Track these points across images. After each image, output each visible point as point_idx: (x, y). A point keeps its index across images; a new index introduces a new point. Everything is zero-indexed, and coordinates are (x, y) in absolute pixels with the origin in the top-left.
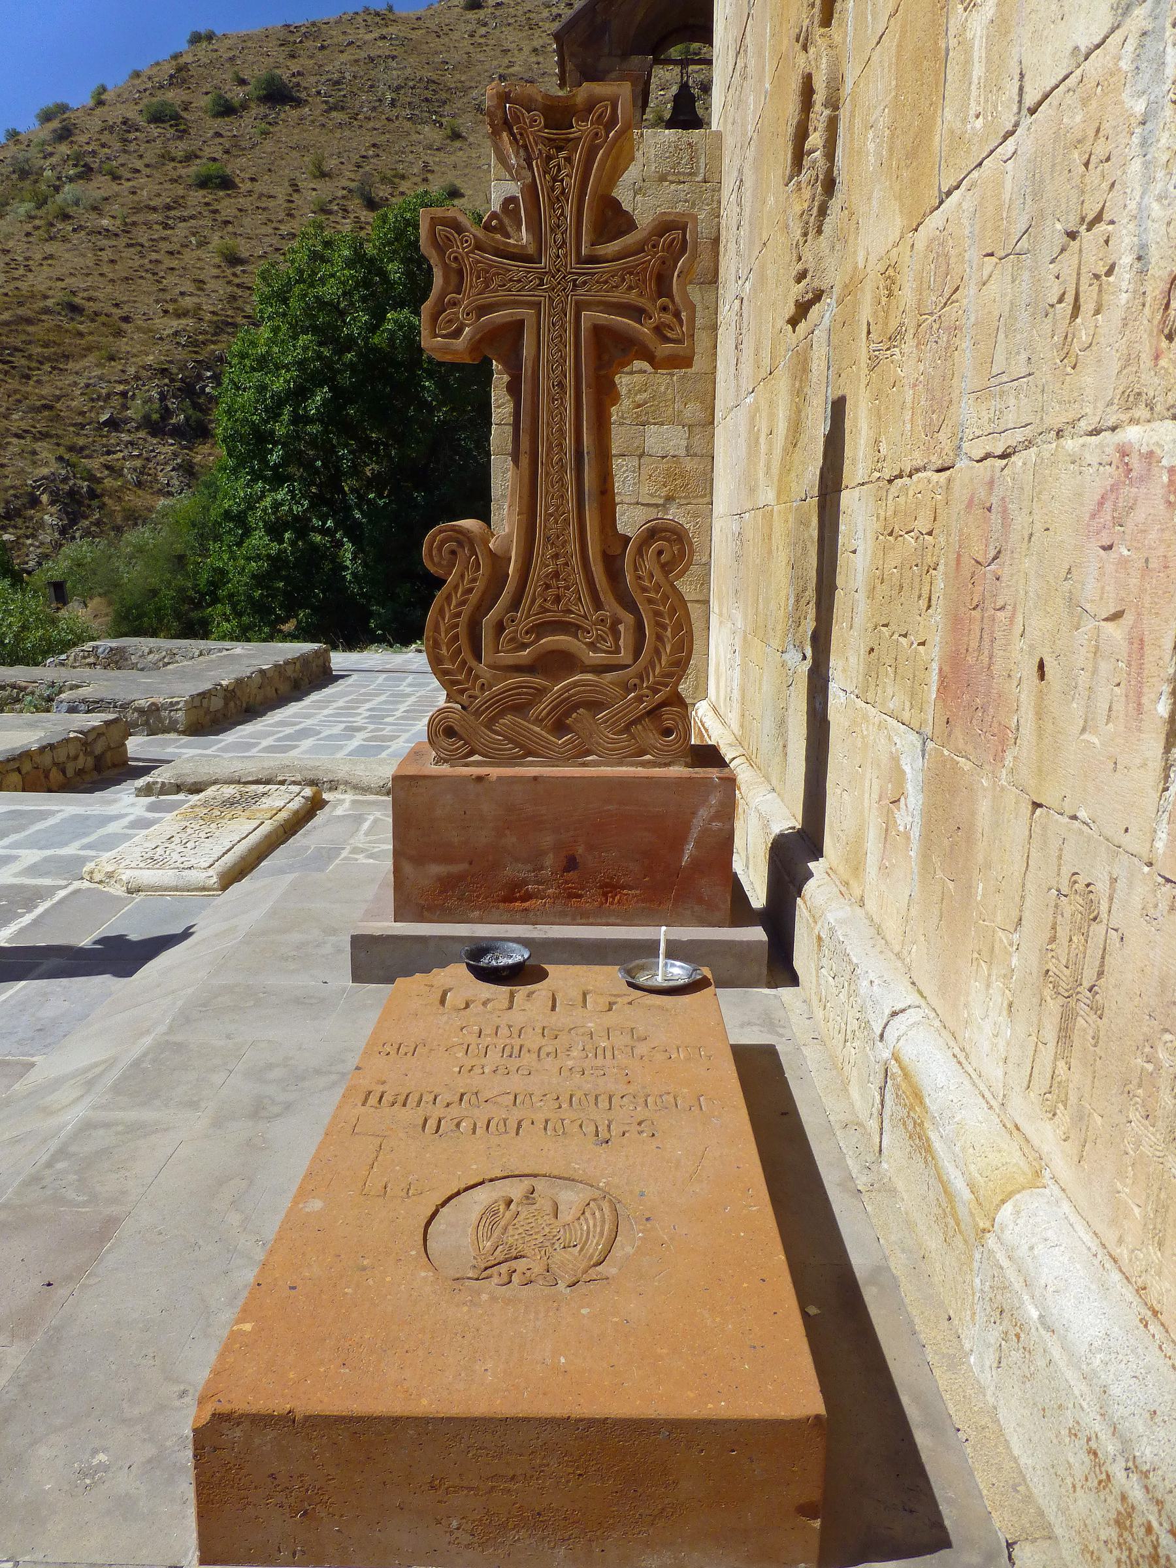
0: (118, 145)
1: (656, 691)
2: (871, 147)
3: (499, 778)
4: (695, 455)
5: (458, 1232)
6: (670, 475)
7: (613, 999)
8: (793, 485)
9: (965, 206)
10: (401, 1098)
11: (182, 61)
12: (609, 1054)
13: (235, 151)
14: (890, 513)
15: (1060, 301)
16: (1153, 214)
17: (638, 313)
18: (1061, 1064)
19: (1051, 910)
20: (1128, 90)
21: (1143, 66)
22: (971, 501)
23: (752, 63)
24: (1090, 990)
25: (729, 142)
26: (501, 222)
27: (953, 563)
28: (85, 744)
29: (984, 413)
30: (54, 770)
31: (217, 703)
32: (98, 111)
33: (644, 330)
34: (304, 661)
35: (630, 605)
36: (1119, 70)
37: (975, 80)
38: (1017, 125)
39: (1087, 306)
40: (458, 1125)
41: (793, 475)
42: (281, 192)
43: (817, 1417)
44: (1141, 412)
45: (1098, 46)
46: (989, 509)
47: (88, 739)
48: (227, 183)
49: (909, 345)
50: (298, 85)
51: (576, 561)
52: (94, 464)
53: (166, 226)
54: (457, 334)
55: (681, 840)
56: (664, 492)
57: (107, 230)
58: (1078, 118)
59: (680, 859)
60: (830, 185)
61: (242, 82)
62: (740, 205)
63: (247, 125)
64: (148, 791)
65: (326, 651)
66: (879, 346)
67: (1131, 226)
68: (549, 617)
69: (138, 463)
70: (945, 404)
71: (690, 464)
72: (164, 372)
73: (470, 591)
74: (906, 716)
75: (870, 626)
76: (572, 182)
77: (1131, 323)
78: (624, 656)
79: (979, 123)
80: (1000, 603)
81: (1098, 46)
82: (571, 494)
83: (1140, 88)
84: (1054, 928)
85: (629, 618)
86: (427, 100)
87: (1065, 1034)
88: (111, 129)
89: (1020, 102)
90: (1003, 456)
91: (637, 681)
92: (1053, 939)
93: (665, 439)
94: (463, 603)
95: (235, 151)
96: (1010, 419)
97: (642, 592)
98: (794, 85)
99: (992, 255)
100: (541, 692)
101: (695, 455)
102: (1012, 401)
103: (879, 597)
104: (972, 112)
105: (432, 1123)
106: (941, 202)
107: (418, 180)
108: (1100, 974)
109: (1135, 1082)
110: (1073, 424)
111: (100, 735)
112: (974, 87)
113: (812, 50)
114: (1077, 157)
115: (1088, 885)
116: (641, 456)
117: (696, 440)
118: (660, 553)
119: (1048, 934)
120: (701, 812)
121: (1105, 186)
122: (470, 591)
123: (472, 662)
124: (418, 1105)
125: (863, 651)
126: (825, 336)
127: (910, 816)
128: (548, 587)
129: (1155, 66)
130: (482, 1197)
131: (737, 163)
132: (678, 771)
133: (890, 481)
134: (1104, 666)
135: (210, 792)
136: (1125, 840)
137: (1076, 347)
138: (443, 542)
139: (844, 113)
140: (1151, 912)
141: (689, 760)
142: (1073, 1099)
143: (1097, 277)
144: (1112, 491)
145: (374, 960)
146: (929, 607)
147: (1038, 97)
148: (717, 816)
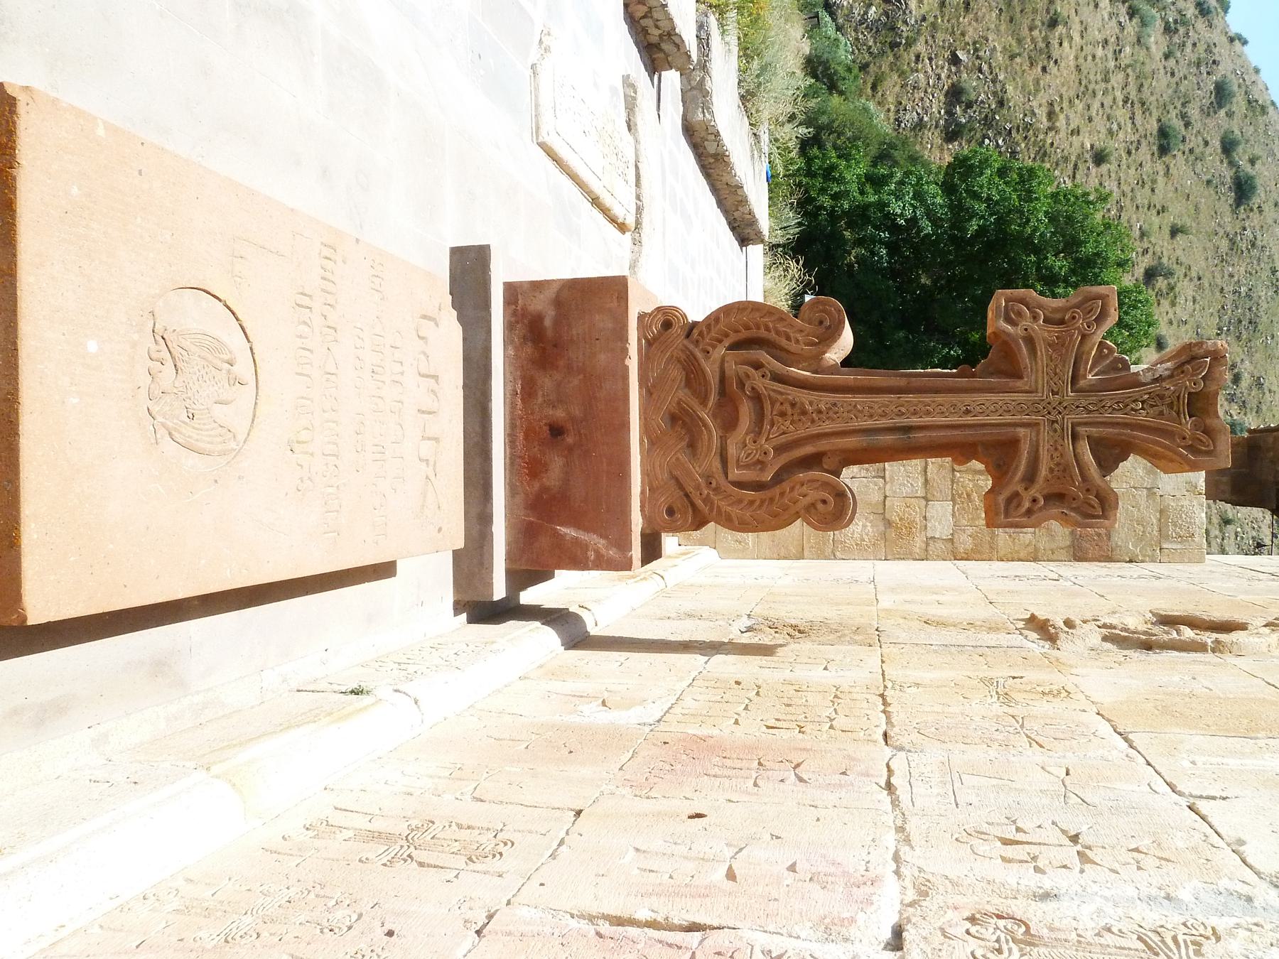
0: (1194, 58)
1: (704, 501)
2: (1176, 679)
3: (626, 368)
4: (927, 545)
5: (197, 317)
6: (910, 526)
7: (431, 463)
8: (892, 622)
9: (1115, 752)
10: (328, 275)
11: (1271, 110)
12: (378, 456)
13: (1192, 158)
14: (855, 696)
15: (1018, 830)
16: (1084, 906)
17: (1030, 478)
18: (350, 834)
19: (485, 826)
20: (1200, 885)
21: (1221, 898)
22: (853, 759)
23: (1261, 585)
24: (409, 856)
25: (1195, 568)
26: (1107, 356)
27: (802, 745)
28: (669, 34)
29: (929, 769)
30: (645, 9)
31: (711, 148)
32: (1224, 39)
33: (1016, 485)
34: (752, 222)
35: (778, 478)
36: (1220, 878)
37: (1225, 761)
38: (1180, 794)
39: (1010, 851)
40: (305, 323)
41: (901, 621)
42: (1158, 200)
43: (25, 619)
44: (911, 895)
45: (1244, 861)
46: (844, 773)
47: (671, 35)
48: (1164, 150)
49: (997, 709)
50: (1252, 210)
51: (814, 430)
52: (920, 47)
53: (1125, 102)
54: (1008, 320)
55: (578, 525)
56: (895, 518)
57: (1120, 51)
58: (1181, 844)
59: (561, 525)
60: (1148, 646)
61: (1252, 162)
62: (1139, 577)
63: (1215, 164)
64: (628, 83)
65: (762, 241)
66: (1000, 686)
67: (1076, 888)
68: (767, 406)
69: (923, 83)
70: (942, 738)
71: (919, 543)
72: (1001, 103)
73: (788, 338)
74: (677, 710)
75: (760, 682)
76: (1142, 417)
77: (990, 888)
78: (735, 473)
79: (1187, 764)
80: (760, 782)
81: (1244, 861)
82: (869, 423)
83: (1202, 895)
84: (469, 828)
85: (768, 476)
86: (1240, 321)
87: (376, 836)
88: (1208, 50)
89: (1201, 797)
90: (889, 786)
91: (714, 485)
92: (460, 826)
93: (941, 518)
94: (778, 333)
95: (1192, 158)
96: (919, 789)
97: (790, 490)
98: (1238, 617)
99: (1067, 774)
100: (704, 402)
101: (927, 545)
102: (935, 791)
103: (785, 688)
104: (1197, 758)
105: (306, 301)
106: (1120, 734)
107: (1171, 315)
108: (421, 864)
109: (322, 893)
110: (907, 840)
111: (677, 46)
112: (1219, 760)
113: (1267, 630)
114: (1144, 843)
115: (501, 854)
116: (926, 499)
117: (940, 545)
118: (824, 502)
119: (465, 823)
120: (602, 541)
121: (1116, 866)
122: (788, 338)
123: (727, 343)
124: (323, 290)
125: (739, 677)
126: (1017, 643)
127: (593, 715)
128: (793, 405)
129: (1220, 908)
130: (235, 340)
131: (1175, 574)
132: (637, 522)
133: (882, 696)
134: (690, 867)
135: (628, 138)
136: (535, 883)
137: (975, 842)
138: (829, 313)
139: (1209, 656)
140: (467, 905)
141: (648, 531)
142: (317, 843)
143: (1034, 858)
144: (844, 872)
145: (469, 268)
146: (768, 727)
147: (1204, 812)
148: (599, 555)
